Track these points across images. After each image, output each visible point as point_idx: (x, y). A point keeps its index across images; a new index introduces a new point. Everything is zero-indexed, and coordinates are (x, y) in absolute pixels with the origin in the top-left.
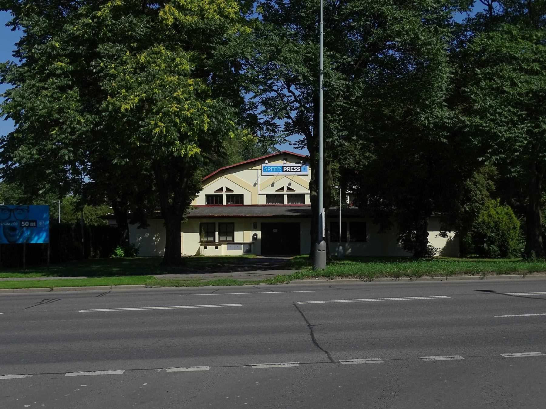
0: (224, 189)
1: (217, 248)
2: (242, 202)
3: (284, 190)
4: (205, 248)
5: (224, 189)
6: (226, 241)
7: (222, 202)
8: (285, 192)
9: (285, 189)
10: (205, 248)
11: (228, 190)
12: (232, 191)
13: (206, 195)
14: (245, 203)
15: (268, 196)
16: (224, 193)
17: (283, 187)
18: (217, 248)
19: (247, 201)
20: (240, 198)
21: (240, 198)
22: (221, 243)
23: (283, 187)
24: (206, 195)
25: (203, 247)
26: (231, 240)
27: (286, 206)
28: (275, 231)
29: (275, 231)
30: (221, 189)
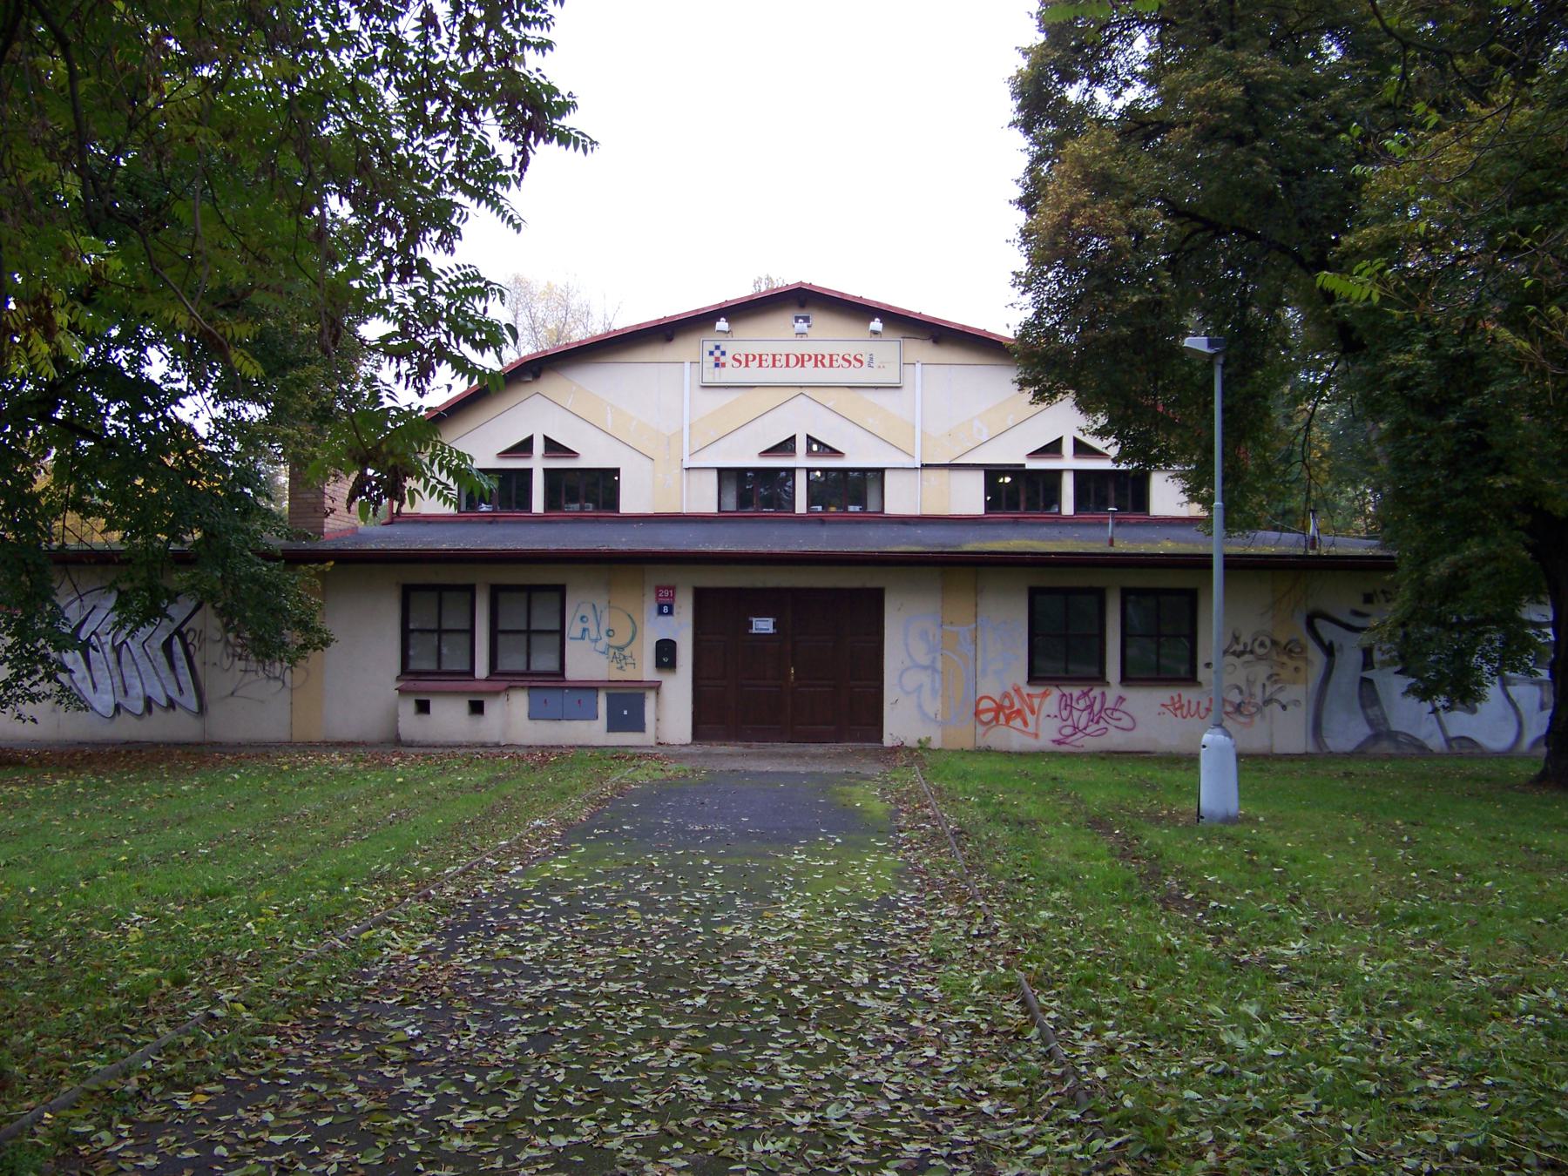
0: (539, 447)
1: (477, 708)
2: (613, 502)
3: (793, 451)
4: (423, 707)
5: (539, 447)
6: (528, 673)
7: (1054, 497)
8: (800, 460)
9: (1068, 447)
10: (423, 707)
11: (552, 447)
12: (570, 453)
13: (616, 471)
14: (627, 505)
15: (992, 473)
16: (538, 464)
17: (1060, 440)
18: (477, 708)
19: (631, 501)
20: (604, 483)
21: (604, 483)
22: (503, 679)
23: (1060, 440)
24: (616, 471)
25: (408, 707)
26: (553, 665)
27: (801, 520)
28: (763, 625)
29: (763, 625)
30: (524, 448)
